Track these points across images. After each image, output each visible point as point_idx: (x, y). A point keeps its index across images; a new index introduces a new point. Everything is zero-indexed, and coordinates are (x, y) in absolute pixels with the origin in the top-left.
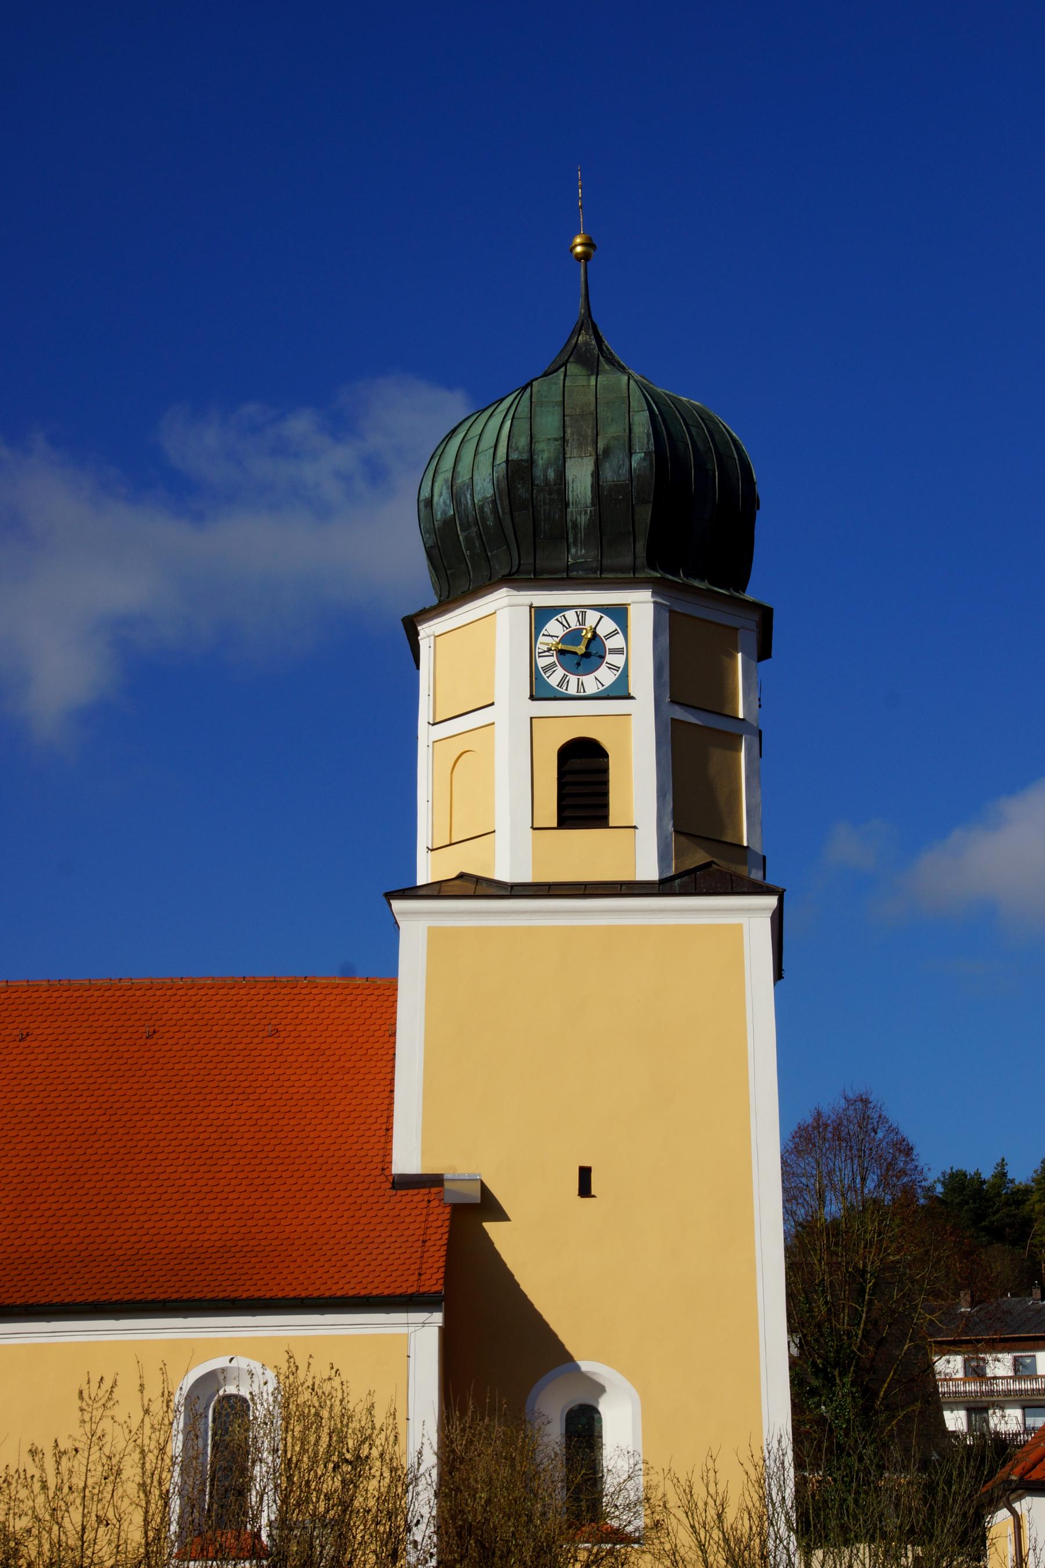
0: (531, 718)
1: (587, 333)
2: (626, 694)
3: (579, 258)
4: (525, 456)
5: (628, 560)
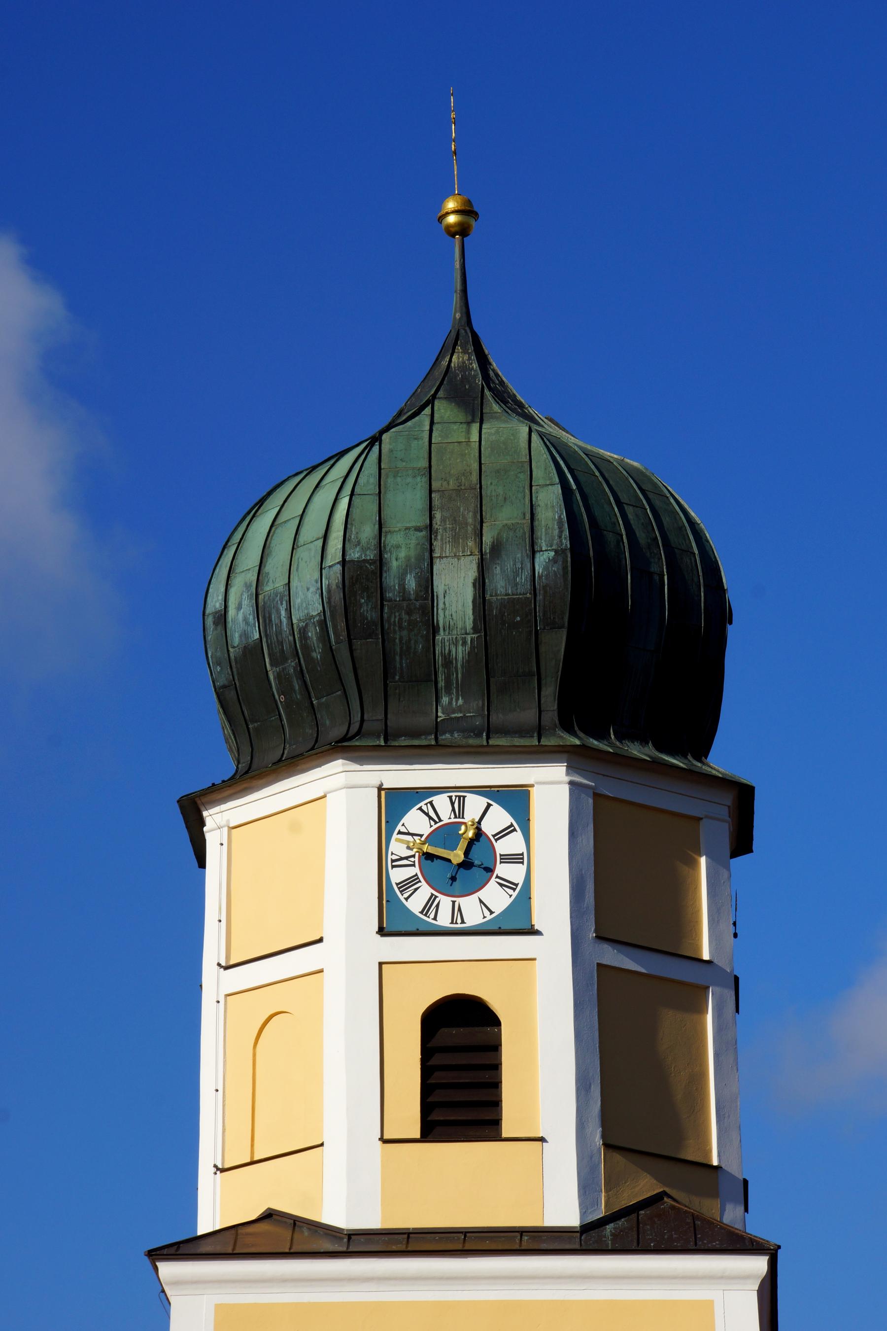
0: (381, 964)
1: (465, 351)
2: (526, 926)
3: (451, 232)
4: (371, 555)
5: (529, 716)
